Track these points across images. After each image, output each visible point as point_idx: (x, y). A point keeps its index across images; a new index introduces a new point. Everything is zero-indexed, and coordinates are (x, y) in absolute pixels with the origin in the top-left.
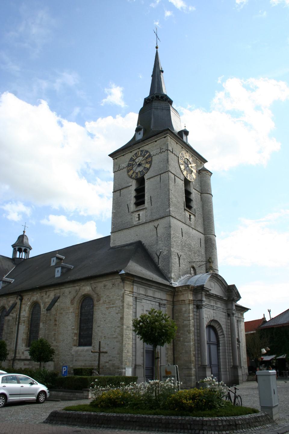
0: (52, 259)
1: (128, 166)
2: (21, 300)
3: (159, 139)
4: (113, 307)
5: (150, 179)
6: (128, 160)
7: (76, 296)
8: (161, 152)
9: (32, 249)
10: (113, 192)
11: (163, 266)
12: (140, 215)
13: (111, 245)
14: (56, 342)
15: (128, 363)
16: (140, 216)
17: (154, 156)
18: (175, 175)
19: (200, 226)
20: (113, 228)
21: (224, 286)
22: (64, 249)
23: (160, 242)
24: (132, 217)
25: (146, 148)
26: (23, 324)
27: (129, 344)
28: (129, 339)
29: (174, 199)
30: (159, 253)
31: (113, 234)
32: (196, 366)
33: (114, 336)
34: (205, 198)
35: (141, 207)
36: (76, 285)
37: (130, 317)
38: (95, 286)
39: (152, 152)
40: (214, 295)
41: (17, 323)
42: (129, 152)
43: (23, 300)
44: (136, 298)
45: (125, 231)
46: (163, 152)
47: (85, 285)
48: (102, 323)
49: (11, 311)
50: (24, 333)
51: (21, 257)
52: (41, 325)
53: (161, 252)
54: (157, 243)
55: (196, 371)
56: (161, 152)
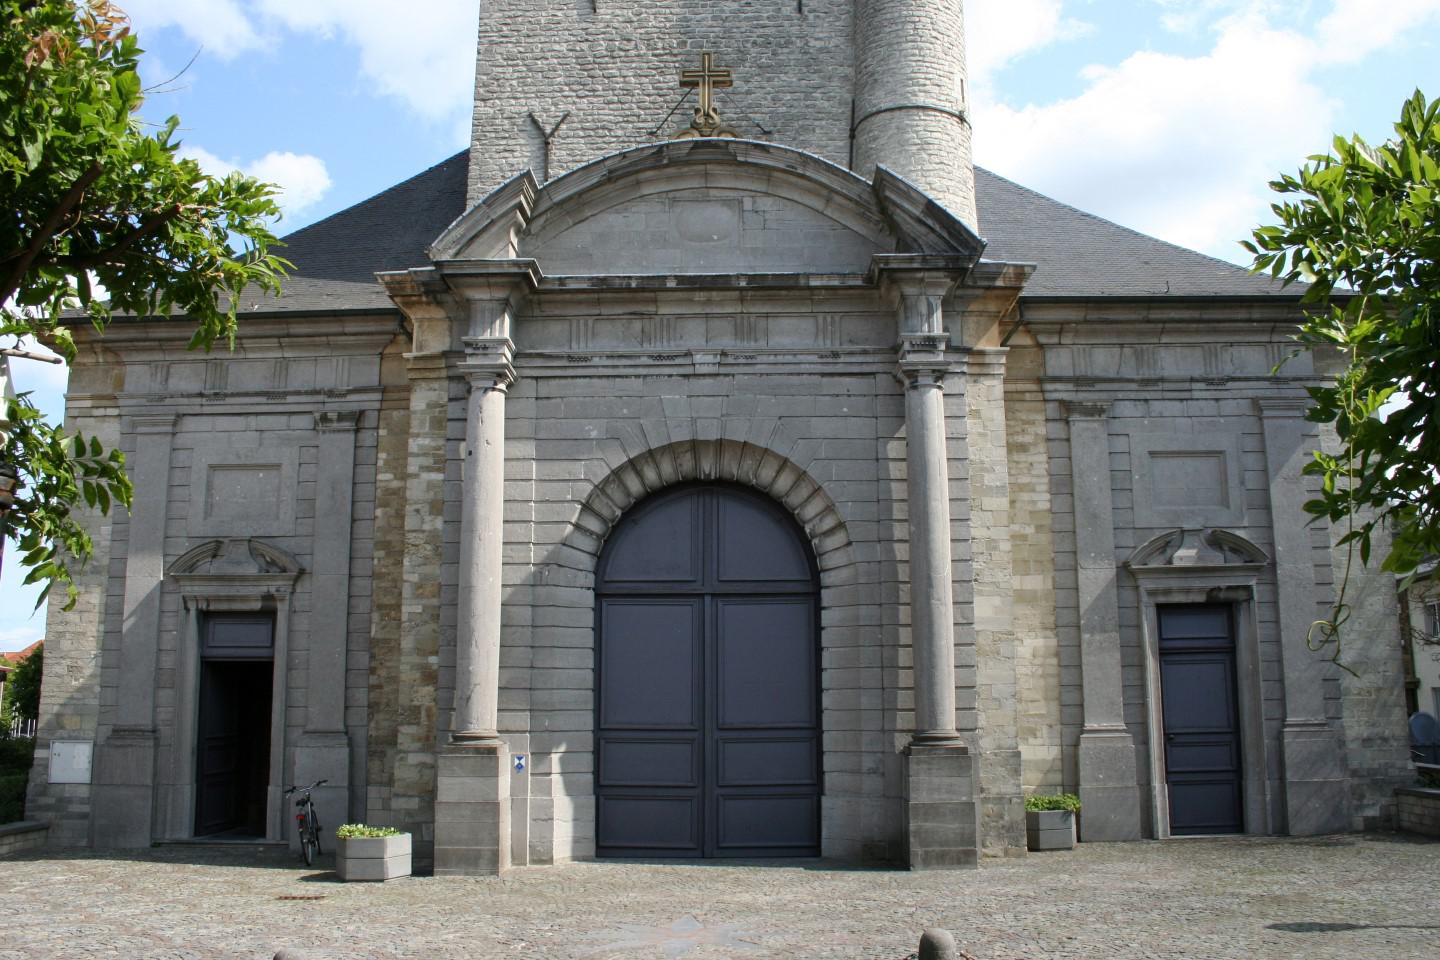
21: (838, 199)
27: (84, 634)
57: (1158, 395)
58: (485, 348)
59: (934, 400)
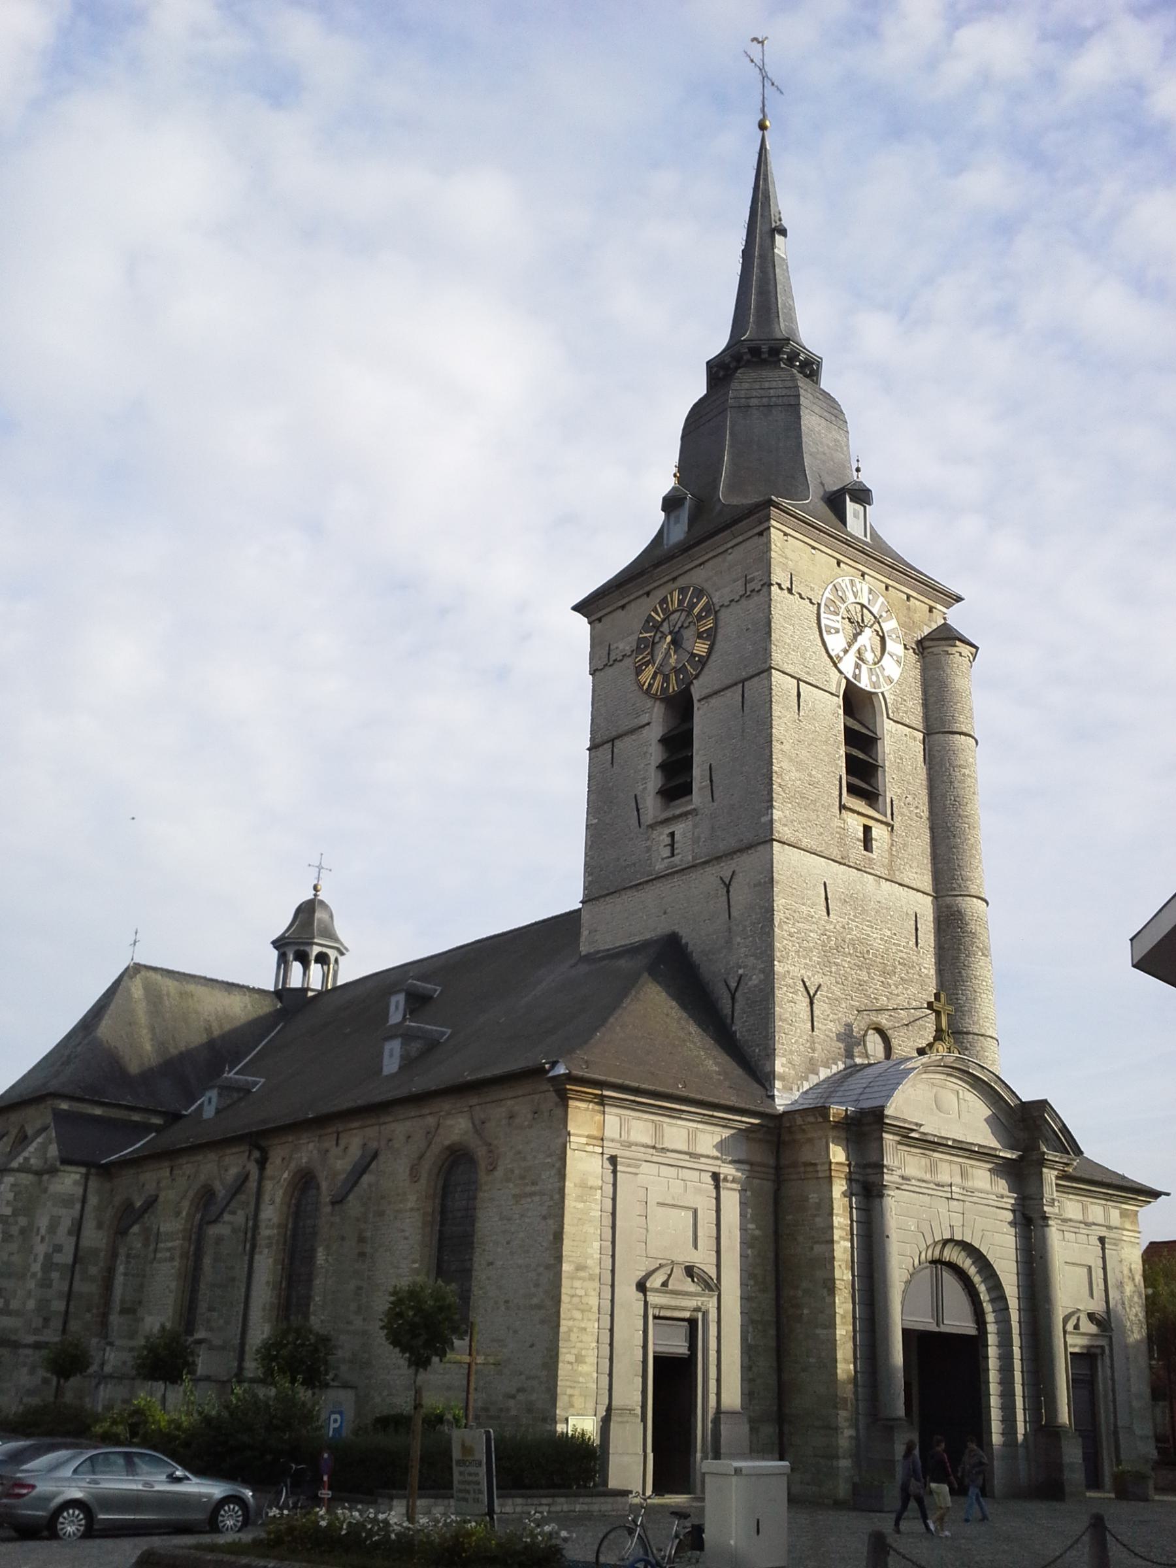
0: (394, 1000)
1: (638, 650)
2: (262, 1163)
3: (741, 542)
4: (532, 1194)
5: (709, 700)
6: (638, 624)
7: (425, 1152)
8: (748, 593)
9: (347, 950)
10: (588, 749)
11: (749, 1030)
12: (677, 837)
13: (584, 949)
14: (364, 1319)
15: (578, 1402)
16: (676, 840)
17: (723, 609)
18: (799, 680)
19: (915, 864)
20: (590, 883)
22: (524, 930)
23: (739, 939)
24: (649, 843)
25: (698, 577)
26: (266, 1251)
27: (585, 1329)
28: (583, 1311)
29: (795, 774)
30: (737, 979)
31: (589, 906)
32: (857, 1419)
33: (535, 1301)
34: (939, 751)
35: (679, 807)
36: (426, 1111)
37: (591, 1230)
38: (483, 1116)
39: (718, 594)
40: (950, 1143)
41: (248, 1246)
42: (641, 592)
43: (268, 1165)
44: (613, 1160)
45: (626, 897)
46: (754, 593)
47: (453, 1111)
48: (499, 1250)
49: (227, 1204)
50: (268, 1283)
51: (306, 986)
52: (321, 1256)
53: (741, 976)
54: (729, 941)
55: (856, 1438)
56: (748, 593)
57: (1068, 1229)
58: (893, 1170)
59: (885, 1183)
